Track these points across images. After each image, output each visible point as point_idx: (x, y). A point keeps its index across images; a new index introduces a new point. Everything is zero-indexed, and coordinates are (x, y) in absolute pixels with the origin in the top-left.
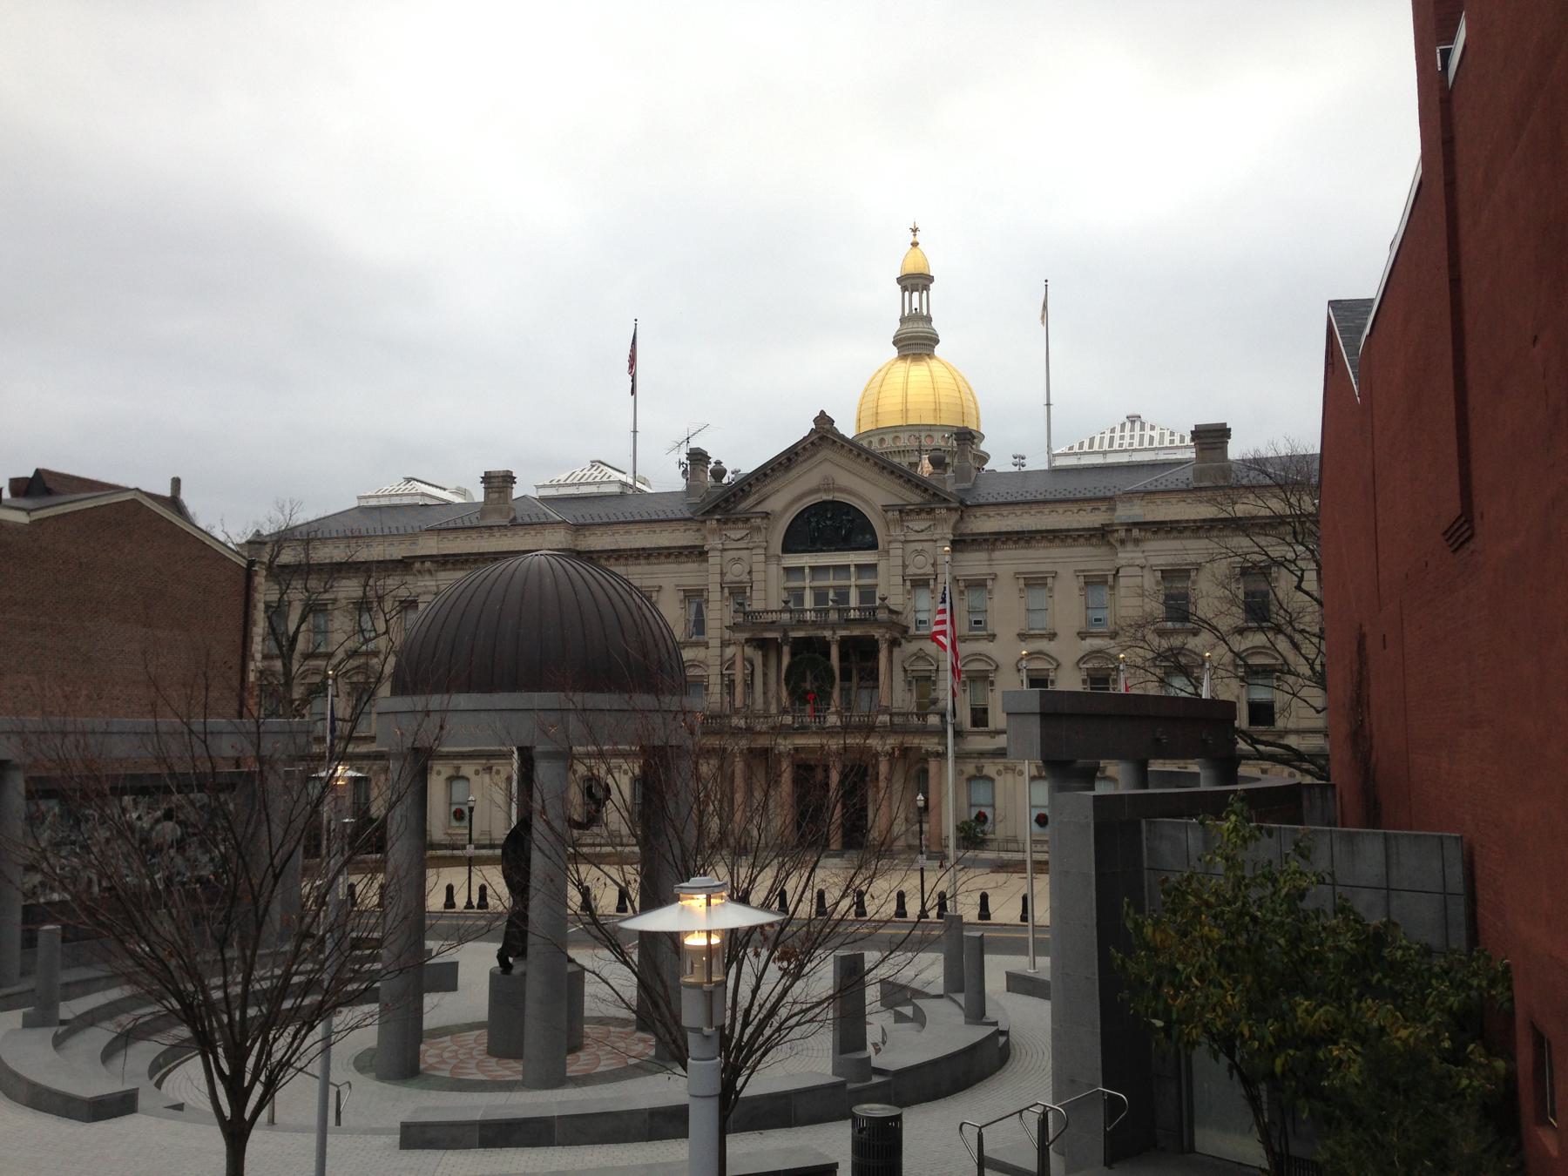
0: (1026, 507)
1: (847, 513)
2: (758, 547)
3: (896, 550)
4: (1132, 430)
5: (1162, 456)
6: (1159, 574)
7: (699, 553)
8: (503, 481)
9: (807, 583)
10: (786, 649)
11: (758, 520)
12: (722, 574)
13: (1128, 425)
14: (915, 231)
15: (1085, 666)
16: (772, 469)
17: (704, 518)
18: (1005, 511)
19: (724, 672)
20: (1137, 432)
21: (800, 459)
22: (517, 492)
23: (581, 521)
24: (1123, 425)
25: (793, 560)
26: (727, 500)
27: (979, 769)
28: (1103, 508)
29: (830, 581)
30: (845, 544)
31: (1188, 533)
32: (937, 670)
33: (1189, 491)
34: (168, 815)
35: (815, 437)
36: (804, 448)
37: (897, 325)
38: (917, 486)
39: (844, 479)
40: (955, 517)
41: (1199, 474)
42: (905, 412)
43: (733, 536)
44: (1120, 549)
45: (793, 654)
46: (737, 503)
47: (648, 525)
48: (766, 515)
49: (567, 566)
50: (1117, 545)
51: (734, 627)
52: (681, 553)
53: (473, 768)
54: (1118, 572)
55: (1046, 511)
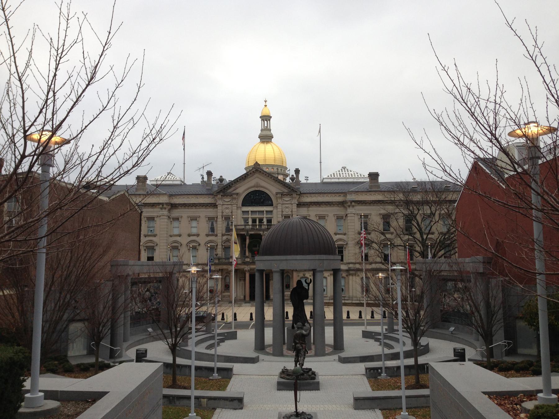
0: (319, 194)
1: (263, 195)
2: (235, 204)
3: (280, 207)
4: (345, 171)
5: (355, 180)
7: (214, 206)
8: (144, 179)
9: (250, 216)
10: (248, 237)
11: (235, 196)
12: (222, 212)
13: (343, 170)
14: (266, 101)
18: (312, 195)
19: (223, 244)
20: (347, 172)
21: (249, 176)
22: (148, 182)
23: (171, 193)
24: (342, 170)
25: (245, 209)
26: (224, 189)
27: (304, 275)
28: (342, 196)
29: (257, 216)
30: (262, 204)
31: (368, 204)
33: (368, 192)
34: (148, 290)
35: (254, 170)
36: (251, 173)
37: (260, 132)
38: (287, 187)
39: (263, 184)
40: (298, 197)
41: (371, 187)
42: (265, 160)
43: (226, 201)
44: (348, 208)
45: (249, 239)
46: (227, 190)
47: (196, 196)
48: (237, 194)
49: (303, 221)
50: (347, 207)
52: (207, 205)
54: (347, 215)
55: (325, 196)
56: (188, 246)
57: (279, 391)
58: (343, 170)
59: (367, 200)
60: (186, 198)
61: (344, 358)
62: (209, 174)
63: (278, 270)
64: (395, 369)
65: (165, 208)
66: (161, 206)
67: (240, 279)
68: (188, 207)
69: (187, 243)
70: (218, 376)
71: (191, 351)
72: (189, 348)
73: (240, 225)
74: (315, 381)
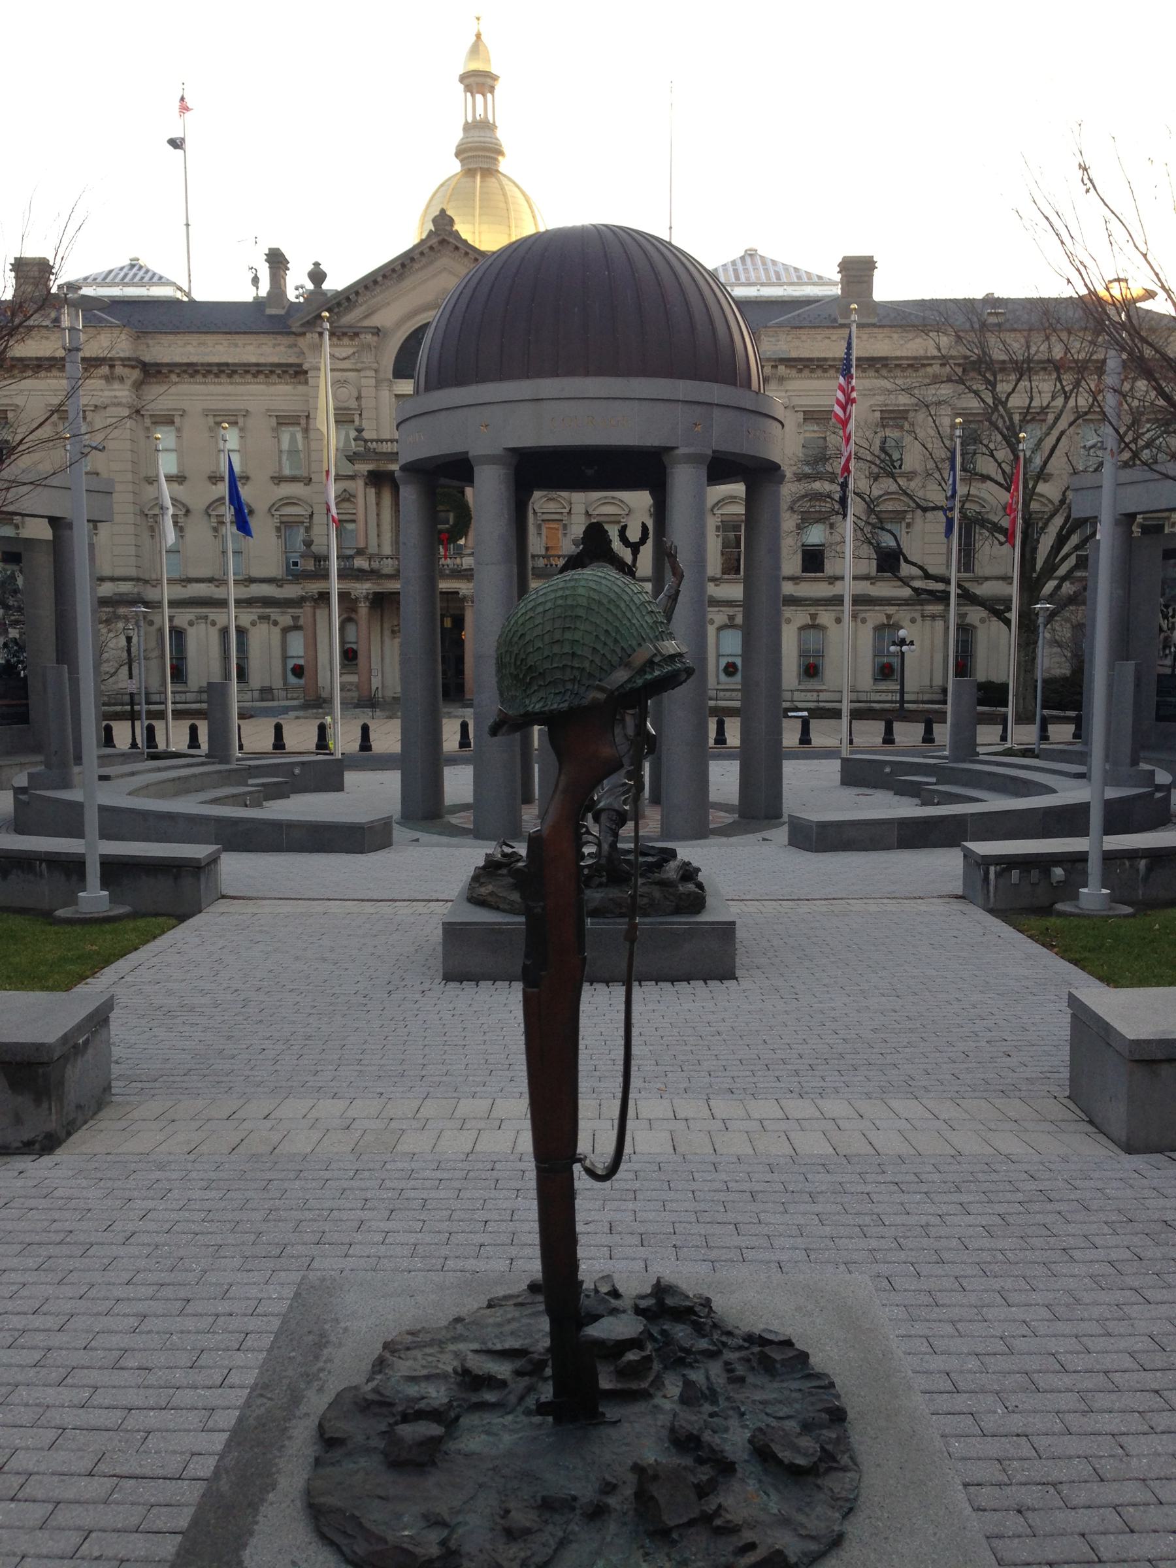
6: (801, 415)
13: (748, 260)
15: (720, 512)
16: (384, 276)
17: (303, 330)
21: (416, 266)
32: (569, 513)
35: (434, 241)
36: (422, 254)
47: (229, 336)
48: (377, 331)
51: (352, 458)
52: (272, 372)
53: (909, 617)
56: (210, 515)
57: (452, 985)
58: (748, 260)
59: (830, 355)
60: (195, 343)
61: (824, 826)
62: (277, 261)
63: (498, 451)
64: (1143, 863)
65: (121, 379)
66: (105, 370)
67: (393, 632)
68: (204, 376)
69: (209, 507)
70: (113, 900)
71: (80, 806)
72: (74, 795)
73: (387, 441)
74: (704, 917)
